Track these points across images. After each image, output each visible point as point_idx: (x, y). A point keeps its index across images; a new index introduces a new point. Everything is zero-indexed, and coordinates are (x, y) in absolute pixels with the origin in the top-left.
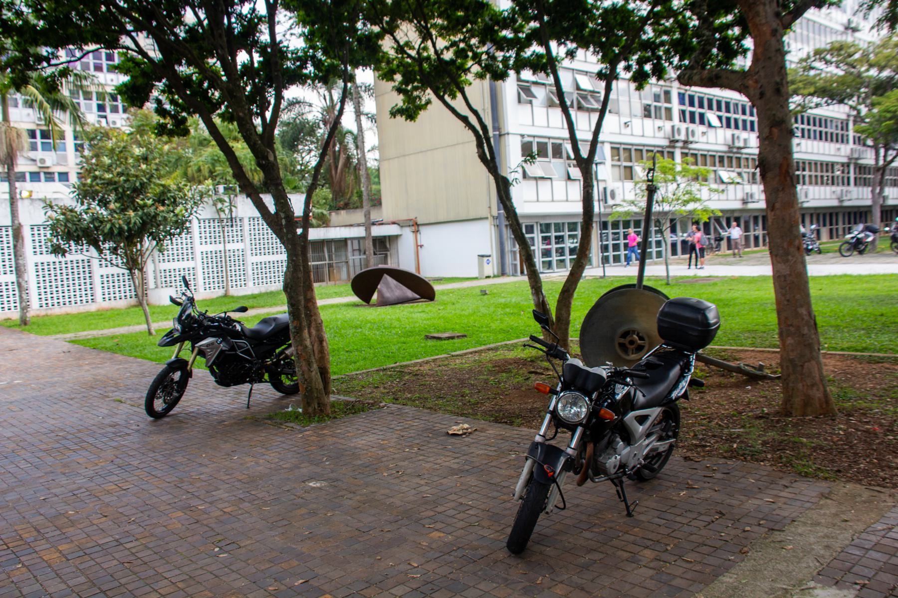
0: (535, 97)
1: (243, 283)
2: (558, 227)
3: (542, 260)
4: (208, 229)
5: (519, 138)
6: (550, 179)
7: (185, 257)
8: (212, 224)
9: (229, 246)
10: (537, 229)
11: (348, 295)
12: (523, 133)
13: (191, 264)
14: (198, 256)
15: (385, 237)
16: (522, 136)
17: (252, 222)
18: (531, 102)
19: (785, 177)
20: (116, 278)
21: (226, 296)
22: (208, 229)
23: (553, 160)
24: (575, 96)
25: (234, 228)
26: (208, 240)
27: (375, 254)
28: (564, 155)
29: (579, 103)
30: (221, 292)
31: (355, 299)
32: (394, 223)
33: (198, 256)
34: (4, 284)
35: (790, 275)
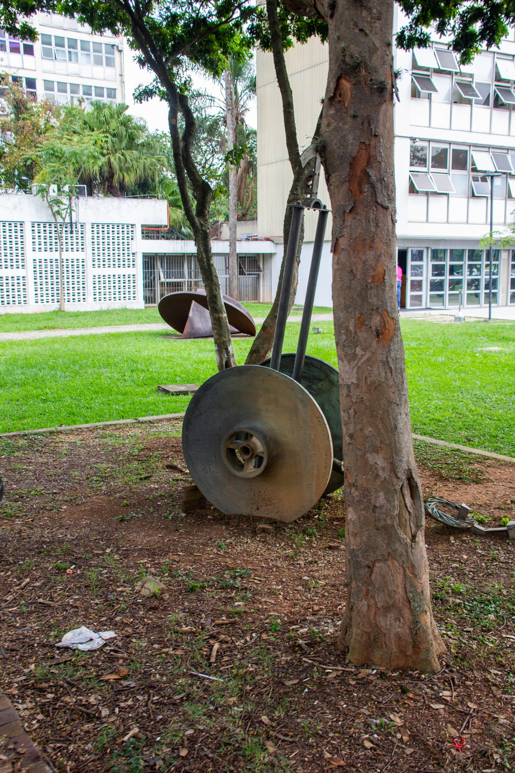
0: (435, 90)
1: (82, 297)
2: (457, 255)
3: (430, 293)
4: (42, 234)
5: (409, 142)
6: (446, 194)
7: (15, 264)
8: (48, 229)
9: (66, 255)
10: (427, 256)
11: (156, 322)
12: (414, 136)
13: (21, 272)
14: (30, 265)
15: (258, 254)
16: (413, 139)
17: (95, 229)
18: (429, 97)
19: (360, 185)
20: (127, 279)
21: (60, 310)
22: (42, 234)
23: (453, 172)
24: (493, 88)
25: (74, 235)
26: (43, 246)
27: (241, 273)
28: (469, 166)
29: (497, 98)
30: (55, 306)
31: (165, 327)
32: (268, 239)
33: (30, 265)
34: (4, 279)
35: (358, 386)
